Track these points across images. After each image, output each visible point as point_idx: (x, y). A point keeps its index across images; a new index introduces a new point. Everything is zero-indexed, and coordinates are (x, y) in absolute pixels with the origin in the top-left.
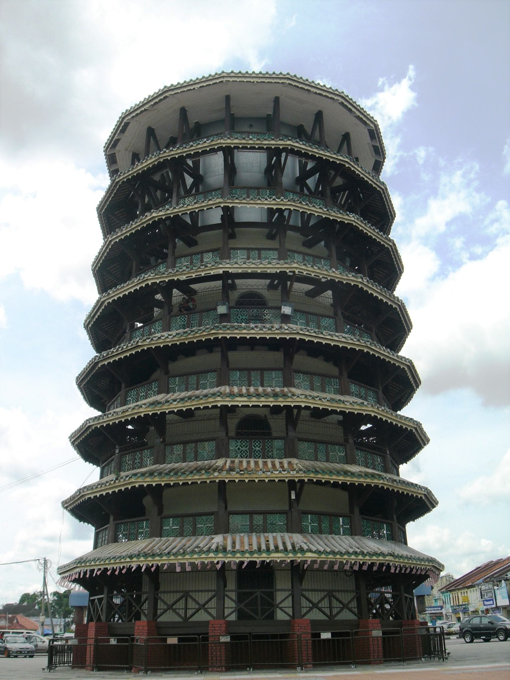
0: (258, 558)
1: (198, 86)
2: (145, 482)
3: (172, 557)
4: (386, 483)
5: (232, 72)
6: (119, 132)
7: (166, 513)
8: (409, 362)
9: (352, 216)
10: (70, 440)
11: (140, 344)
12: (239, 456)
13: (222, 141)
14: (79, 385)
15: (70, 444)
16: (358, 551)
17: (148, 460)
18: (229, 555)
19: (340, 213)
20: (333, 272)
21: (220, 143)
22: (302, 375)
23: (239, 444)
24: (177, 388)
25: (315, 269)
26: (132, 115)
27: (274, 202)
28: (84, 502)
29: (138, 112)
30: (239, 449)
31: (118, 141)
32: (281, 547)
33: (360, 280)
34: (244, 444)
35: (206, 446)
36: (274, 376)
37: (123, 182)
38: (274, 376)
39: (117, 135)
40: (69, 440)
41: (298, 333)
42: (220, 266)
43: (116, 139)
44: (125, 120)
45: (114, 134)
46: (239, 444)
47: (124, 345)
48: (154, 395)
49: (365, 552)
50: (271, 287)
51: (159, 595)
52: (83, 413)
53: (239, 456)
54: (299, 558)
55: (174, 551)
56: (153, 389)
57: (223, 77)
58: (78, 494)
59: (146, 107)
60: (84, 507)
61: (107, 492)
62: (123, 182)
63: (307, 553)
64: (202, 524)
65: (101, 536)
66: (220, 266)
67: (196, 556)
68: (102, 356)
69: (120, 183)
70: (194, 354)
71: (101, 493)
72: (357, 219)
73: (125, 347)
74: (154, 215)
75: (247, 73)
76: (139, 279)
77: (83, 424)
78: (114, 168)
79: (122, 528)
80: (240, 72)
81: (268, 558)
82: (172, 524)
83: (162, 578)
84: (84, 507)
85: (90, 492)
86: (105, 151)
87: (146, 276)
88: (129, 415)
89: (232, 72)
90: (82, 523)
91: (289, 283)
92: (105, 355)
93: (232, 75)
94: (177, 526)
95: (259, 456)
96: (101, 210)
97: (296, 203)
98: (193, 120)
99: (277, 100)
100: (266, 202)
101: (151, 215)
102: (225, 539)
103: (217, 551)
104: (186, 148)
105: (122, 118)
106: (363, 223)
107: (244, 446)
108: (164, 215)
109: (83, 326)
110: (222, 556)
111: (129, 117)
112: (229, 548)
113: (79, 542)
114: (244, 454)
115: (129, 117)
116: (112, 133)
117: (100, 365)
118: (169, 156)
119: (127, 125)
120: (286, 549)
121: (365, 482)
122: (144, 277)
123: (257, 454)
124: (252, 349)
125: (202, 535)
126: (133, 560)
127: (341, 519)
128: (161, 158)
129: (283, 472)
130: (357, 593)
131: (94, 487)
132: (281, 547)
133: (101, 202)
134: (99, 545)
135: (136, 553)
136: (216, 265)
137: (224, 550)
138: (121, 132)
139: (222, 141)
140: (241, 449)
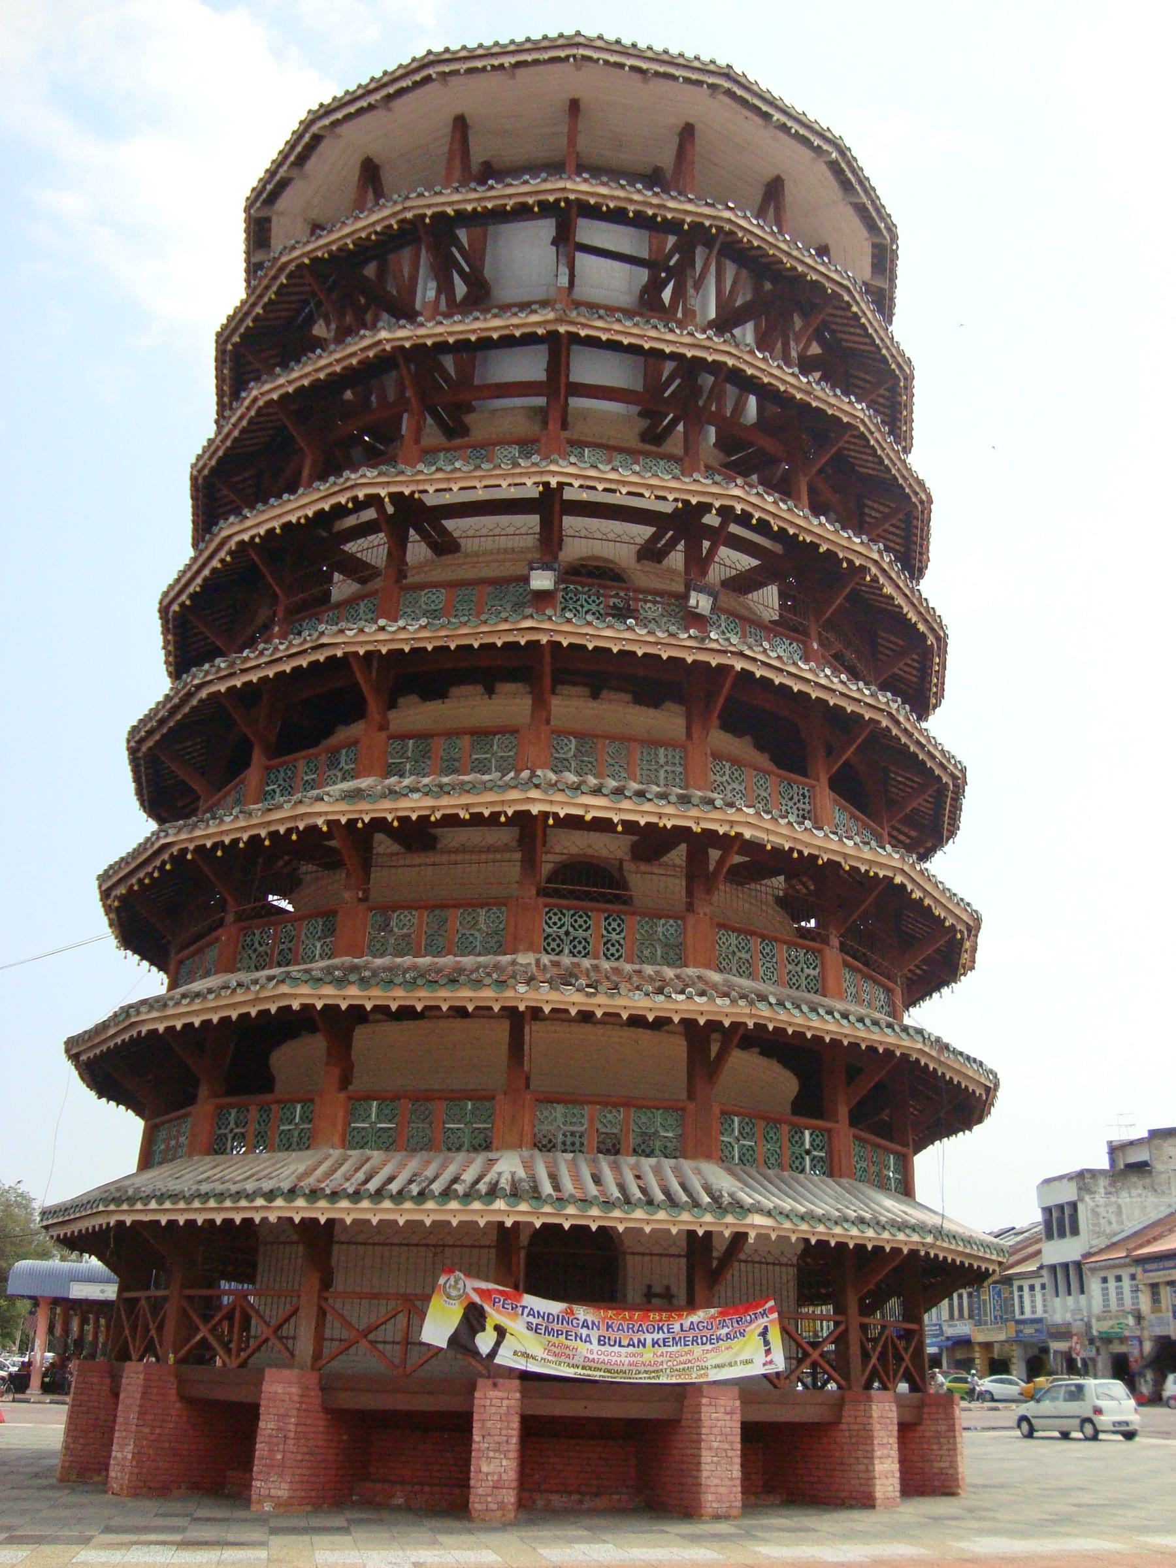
0: (621, 1220)
1: (513, 60)
2: (320, 997)
3: (387, 1204)
4: (927, 1049)
5: (600, 38)
6: (292, 158)
7: (359, 1084)
8: (961, 770)
9: (859, 407)
10: (100, 887)
11: (325, 640)
12: (566, 951)
13: (569, 185)
14: (133, 752)
15: (98, 897)
16: (868, 1216)
17: (318, 945)
18: (547, 1209)
19: (835, 395)
20: (820, 524)
21: (564, 189)
22: (728, 765)
23: (567, 920)
24: (408, 766)
25: (781, 509)
26: (333, 118)
27: (688, 340)
28: (137, 1041)
29: (352, 109)
30: (567, 933)
31: (283, 184)
32: (659, 1196)
33: (876, 556)
34: (580, 921)
35: (481, 919)
36: (662, 760)
37: (299, 267)
38: (662, 760)
39: (285, 167)
40: (96, 883)
41: (741, 654)
42: (553, 468)
43: (282, 178)
44: (315, 129)
45: (278, 164)
46: (567, 920)
47: (281, 643)
48: (344, 779)
49: (883, 1219)
50: (650, 553)
51: (331, 1301)
52: (129, 827)
53: (566, 951)
54: (594, 1219)
55: (394, 1187)
56: (343, 764)
57: (578, 45)
58: (121, 1018)
59: (372, 99)
60: (117, 1063)
61: (206, 1017)
62: (301, 266)
63: (750, 1215)
64: (459, 1122)
65: (162, 1134)
66: (553, 468)
67: (476, 1205)
68: (214, 670)
69: (292, 267)
70: (443, 695)
71: (188, 1020)
72: (870, 417)
73: (282, 647)
74: (384, 335)
75: (634, 46)
76: (335, 483)
77: (148, 839)
78: (258, 257)
79: (232, 1119)
80: (618, 42)
81: (648, 1222)
82: (378, 1115)
83: (338, 1255)
84: (117, 1063)
85: (155, 1014)
86: (247, 209)
87: (353, 476)
88: (282, 821)
89: (600, 38)
90: (104, 1100)
91: (706, 544)
92: (223, 665)
93: (599, 43)
94: (390, 1121)
95: (617, 955)
96: (226, 342)
97: (741, 351)
98: (479, 153)
99: (688, 132)
100: (670, 337)
101: (375, 335)
102: (528, 1166)
103: (515, 1194)
104: (475, 190)
105: (307, 125)
106: (879, 430)
107: (580, 926)
108: (408, 338)
109: (157, 606)
110: (529, 1209)
111: (326, 122)
112: (547, 1188)
113: (96, 1147)
114: (580, 947)
115: (326, 122)
116: (273, 162)
117: (204, 694)
118: (429, 206)
119: (317, 139)
120: (696, 1204)
121: (881, 1043)
122: (348, 479)
123: (613, 950)
124: (595, 696)
125: (458, 1149)
126: (273, 1204)
127: (807, 1133)
128: (410, 209)
129: (697, 999)
130: (837, 1324)
131: (171, 1003)
132: (659, 1196)
133: (230, 319)
134: (157, 1158)
135: (286, 1186)
136: (544, 463)
137: (535, 1194)
138: (293, 164)
139: (569, 185)
140: (576, 934)
